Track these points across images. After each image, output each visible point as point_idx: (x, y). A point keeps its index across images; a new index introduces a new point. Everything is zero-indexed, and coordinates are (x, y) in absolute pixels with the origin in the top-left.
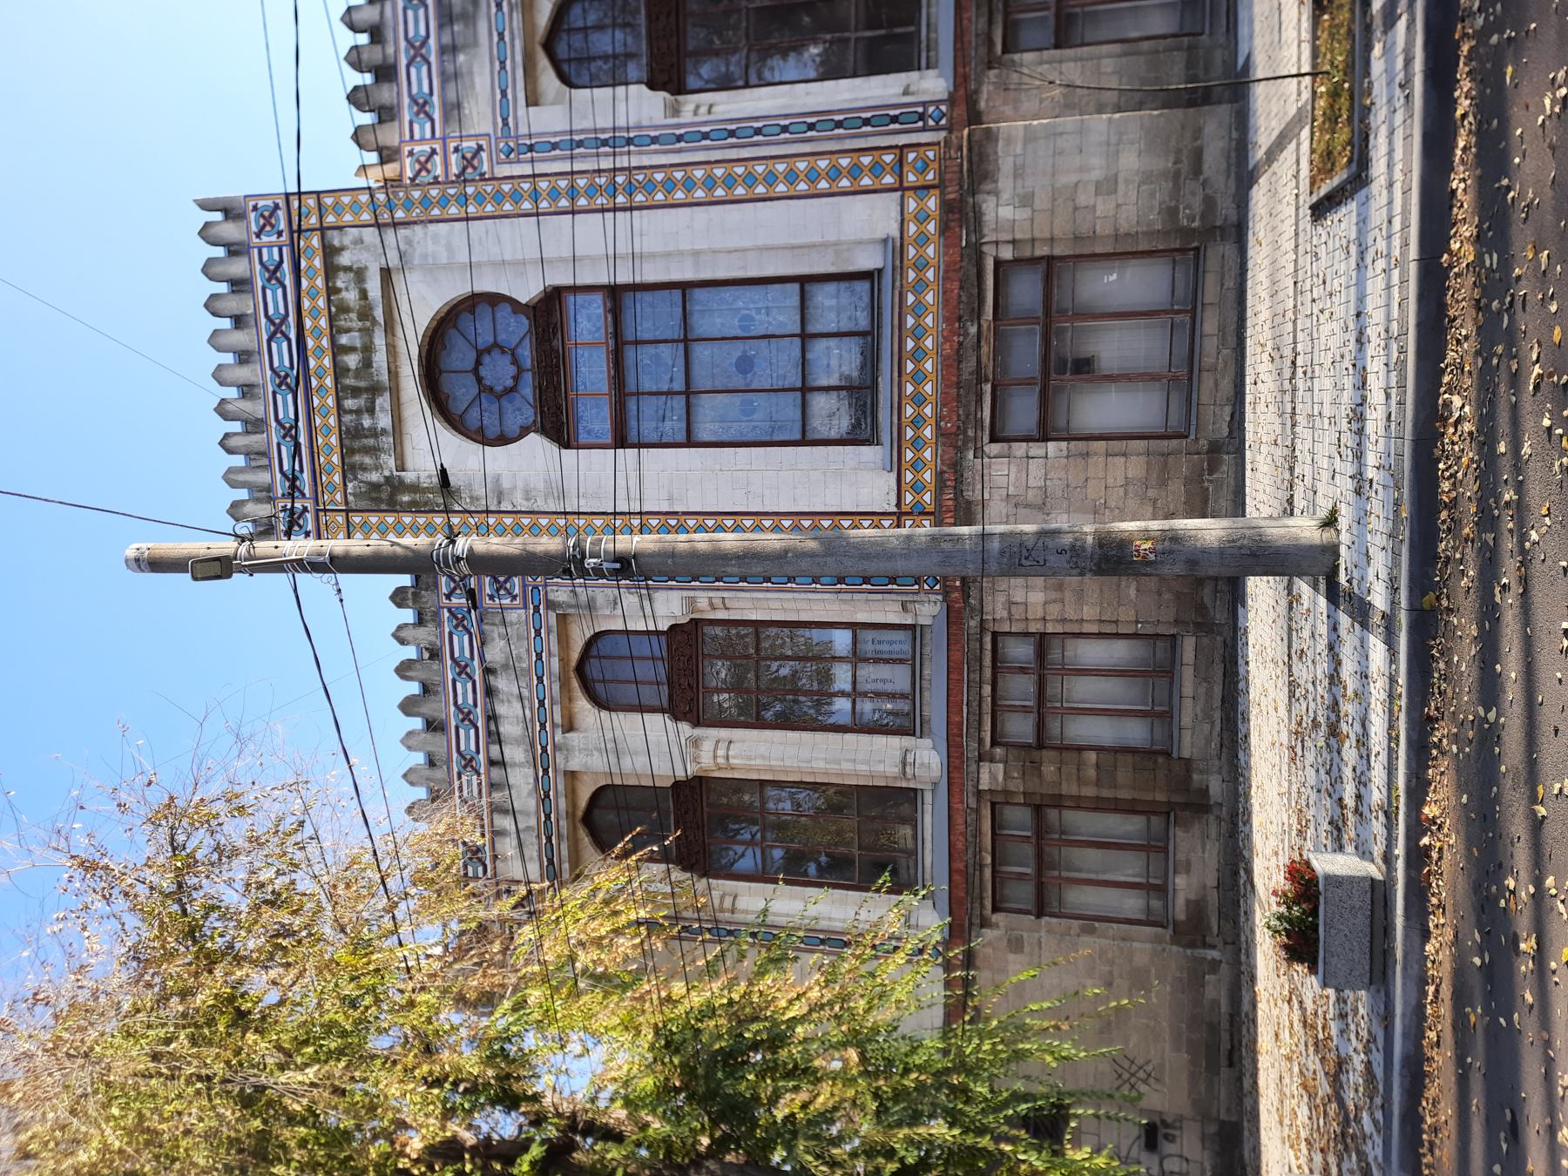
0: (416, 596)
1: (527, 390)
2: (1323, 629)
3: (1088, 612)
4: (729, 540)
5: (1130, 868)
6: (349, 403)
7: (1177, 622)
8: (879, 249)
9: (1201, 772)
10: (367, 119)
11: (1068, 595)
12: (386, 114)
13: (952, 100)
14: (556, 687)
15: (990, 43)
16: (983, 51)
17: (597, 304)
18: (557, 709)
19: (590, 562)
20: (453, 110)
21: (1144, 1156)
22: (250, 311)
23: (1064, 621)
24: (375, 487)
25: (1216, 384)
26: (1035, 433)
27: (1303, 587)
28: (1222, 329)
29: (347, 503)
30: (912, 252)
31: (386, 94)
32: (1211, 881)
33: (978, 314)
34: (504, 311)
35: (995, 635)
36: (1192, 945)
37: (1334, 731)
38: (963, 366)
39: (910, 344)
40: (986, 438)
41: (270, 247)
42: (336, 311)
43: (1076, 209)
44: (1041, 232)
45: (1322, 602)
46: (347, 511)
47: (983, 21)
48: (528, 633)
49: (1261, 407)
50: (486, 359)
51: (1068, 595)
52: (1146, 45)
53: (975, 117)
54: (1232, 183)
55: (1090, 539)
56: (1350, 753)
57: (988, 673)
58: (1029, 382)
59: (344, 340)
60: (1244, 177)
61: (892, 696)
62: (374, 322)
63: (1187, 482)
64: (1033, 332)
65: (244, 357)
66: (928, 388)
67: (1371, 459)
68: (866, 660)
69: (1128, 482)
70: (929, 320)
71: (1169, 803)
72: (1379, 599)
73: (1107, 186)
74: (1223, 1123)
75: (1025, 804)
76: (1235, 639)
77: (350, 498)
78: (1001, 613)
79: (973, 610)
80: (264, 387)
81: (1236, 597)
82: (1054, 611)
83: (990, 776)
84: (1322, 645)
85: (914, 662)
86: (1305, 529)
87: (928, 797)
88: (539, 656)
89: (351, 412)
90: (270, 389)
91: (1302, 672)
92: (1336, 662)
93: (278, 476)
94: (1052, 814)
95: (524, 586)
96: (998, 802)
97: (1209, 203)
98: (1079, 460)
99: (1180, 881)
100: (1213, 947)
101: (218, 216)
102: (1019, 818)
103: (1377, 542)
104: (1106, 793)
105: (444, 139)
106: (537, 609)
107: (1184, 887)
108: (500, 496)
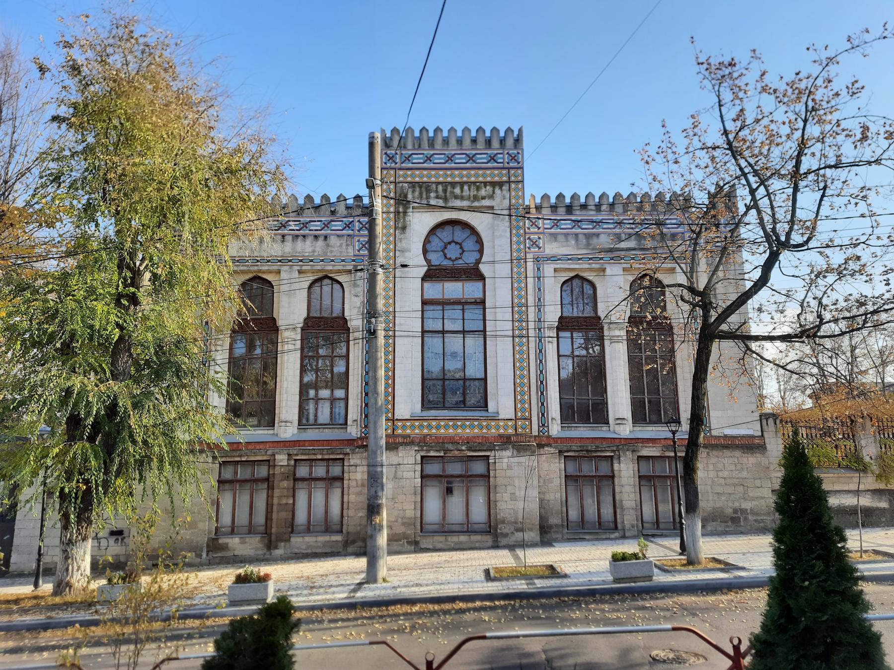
0: (359, 206)
1: (446, 263)
2: (348, 582)
3: (352, 498)
4: (381, 373)
5: (243, 518)
6: (440, 188)
7: (348, 533)
8: (495, 411)
9: (285, 546)
10: (553, 200)
11: (359, 489)
12: (554, 208)
13: (549, 437)
14: (319, 268)
15: (568, 451)
16: (565, 449)
17: (479, 295)
18: (309, 268)
19: (373, 320)
20: (554, 237)
21: (107, 531)
22: (478, 147)
23: (349, 488)
24: (406, 196)
25: (441, 542)
26: (424, 473)
27: (363, 575)
28: (461, 543)
29: (399, 183)
30: (493, 424)
31: (562, 210)
32: (236, 553)
33: (470, 449)
34: (476, 255)
35: (343, 459)
36: (208, 546)
37: (312, 588)
38: (451, 445)
39: (459, 423)
40: (423, 454)
41: (503, 158)
42: (477, 185)
43: (506, 486)
44: (498, 473)
45: (358, 581)
46: (395, 182)
47: (575, 448)
48: (343, 256)
49: (429, 558)
50: (458, 246)
51: (359, 489)
52: (565, 509)
53: (540, 446)
54: (513, 543)
55: (380, 502)
56: (306, 592)
57: (327, 457)
58: (444, 470)
59: (466, 188)
60: (511, 548)
61: (316, 416)
62: (473, 202)
63: (404, 533)
64: (463, 471)
65: (460, 142)
66: (442, 431)
67: (404, 590)
68: (332, 404)
69: (404, 511)
70: (468, 431)
71: (271, 534)
72: (359, 594)
73: (513, 497)
74: (126, 564)
75: (269, 474)
76: (341, 556)
77: (401, 184)
78: (352, 462)
79: (353, 450)
80: (447, 150)
81: (358, 554)
82: (353, 484)
83: (282, 459)
84: (342, 582)
85: (332, 423)
86: (382, 572)
87: (271, 432)
88: (332, 261)
89: (437, 188)
90: (446, 152)
91: (332, 578)
92: (337, 586)
93: (410, 152)
94: (265, 486)
95: (363, 256)
96: (270, 463)
97: (506, 535)
98: (413, 491)
99: (236, 540)
100: (207, 555)
101: (515, 135)
102: (262, 472)
103: (377, 593)
104: (275, 508)
105: (543, 233)
106: (354, 261)
107: (234, 542)
108: (402, 251)
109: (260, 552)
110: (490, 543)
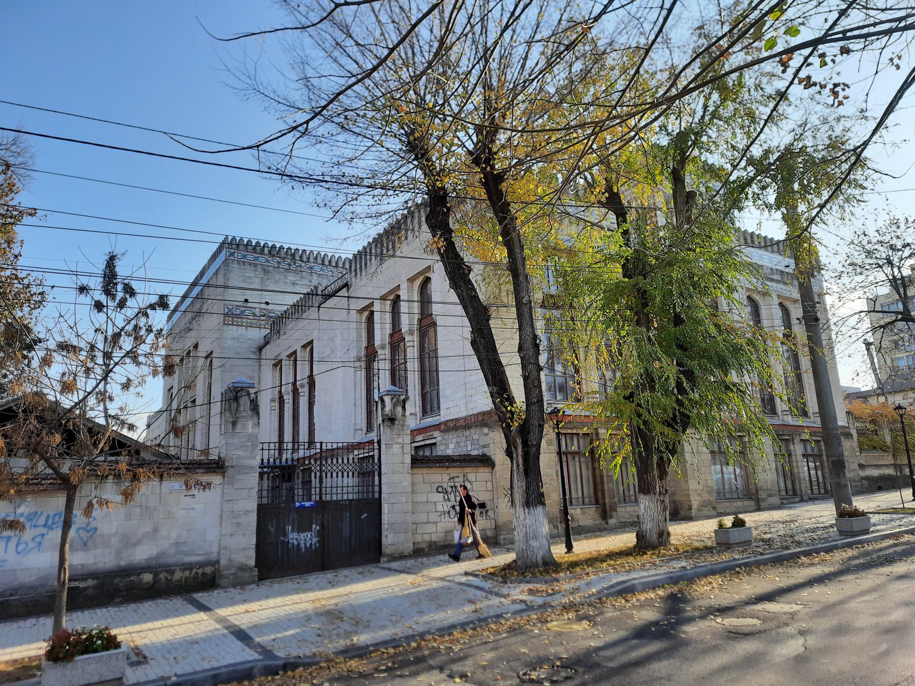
28: (739, 507)
32: (581, 523)
97: (764, 500)
104: (605, 479)
109: (597, 522)
110: (753, 508)
